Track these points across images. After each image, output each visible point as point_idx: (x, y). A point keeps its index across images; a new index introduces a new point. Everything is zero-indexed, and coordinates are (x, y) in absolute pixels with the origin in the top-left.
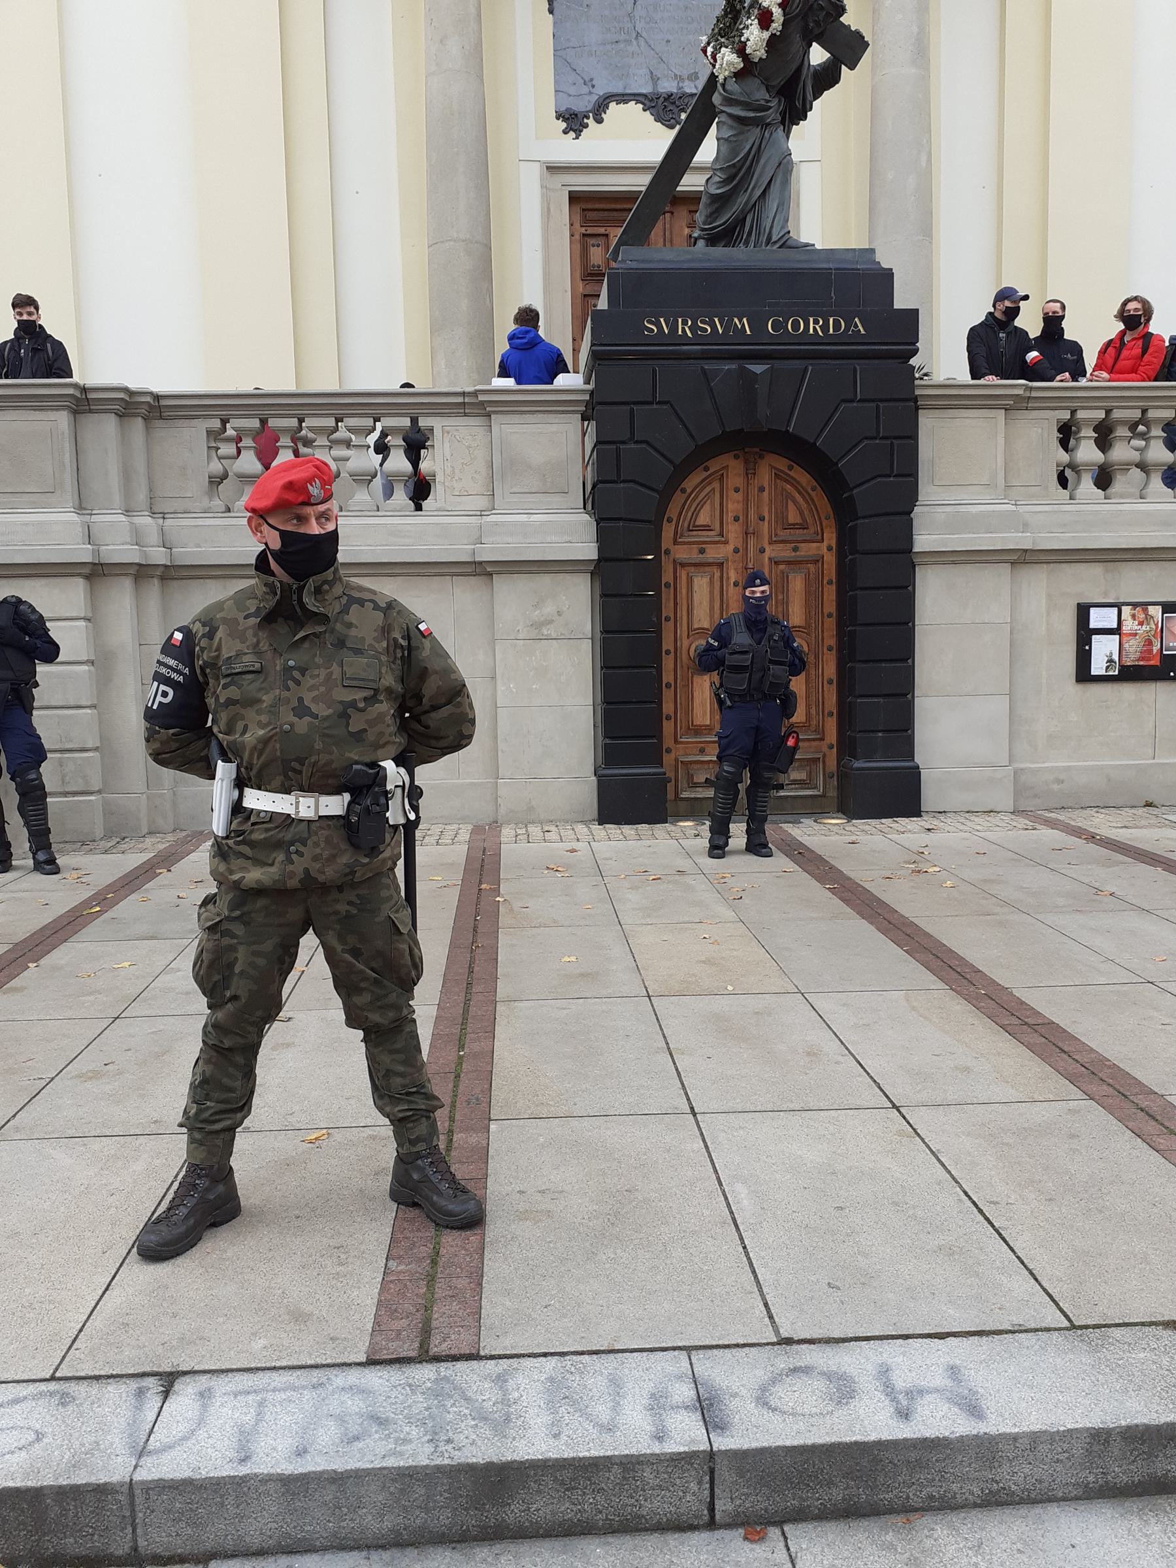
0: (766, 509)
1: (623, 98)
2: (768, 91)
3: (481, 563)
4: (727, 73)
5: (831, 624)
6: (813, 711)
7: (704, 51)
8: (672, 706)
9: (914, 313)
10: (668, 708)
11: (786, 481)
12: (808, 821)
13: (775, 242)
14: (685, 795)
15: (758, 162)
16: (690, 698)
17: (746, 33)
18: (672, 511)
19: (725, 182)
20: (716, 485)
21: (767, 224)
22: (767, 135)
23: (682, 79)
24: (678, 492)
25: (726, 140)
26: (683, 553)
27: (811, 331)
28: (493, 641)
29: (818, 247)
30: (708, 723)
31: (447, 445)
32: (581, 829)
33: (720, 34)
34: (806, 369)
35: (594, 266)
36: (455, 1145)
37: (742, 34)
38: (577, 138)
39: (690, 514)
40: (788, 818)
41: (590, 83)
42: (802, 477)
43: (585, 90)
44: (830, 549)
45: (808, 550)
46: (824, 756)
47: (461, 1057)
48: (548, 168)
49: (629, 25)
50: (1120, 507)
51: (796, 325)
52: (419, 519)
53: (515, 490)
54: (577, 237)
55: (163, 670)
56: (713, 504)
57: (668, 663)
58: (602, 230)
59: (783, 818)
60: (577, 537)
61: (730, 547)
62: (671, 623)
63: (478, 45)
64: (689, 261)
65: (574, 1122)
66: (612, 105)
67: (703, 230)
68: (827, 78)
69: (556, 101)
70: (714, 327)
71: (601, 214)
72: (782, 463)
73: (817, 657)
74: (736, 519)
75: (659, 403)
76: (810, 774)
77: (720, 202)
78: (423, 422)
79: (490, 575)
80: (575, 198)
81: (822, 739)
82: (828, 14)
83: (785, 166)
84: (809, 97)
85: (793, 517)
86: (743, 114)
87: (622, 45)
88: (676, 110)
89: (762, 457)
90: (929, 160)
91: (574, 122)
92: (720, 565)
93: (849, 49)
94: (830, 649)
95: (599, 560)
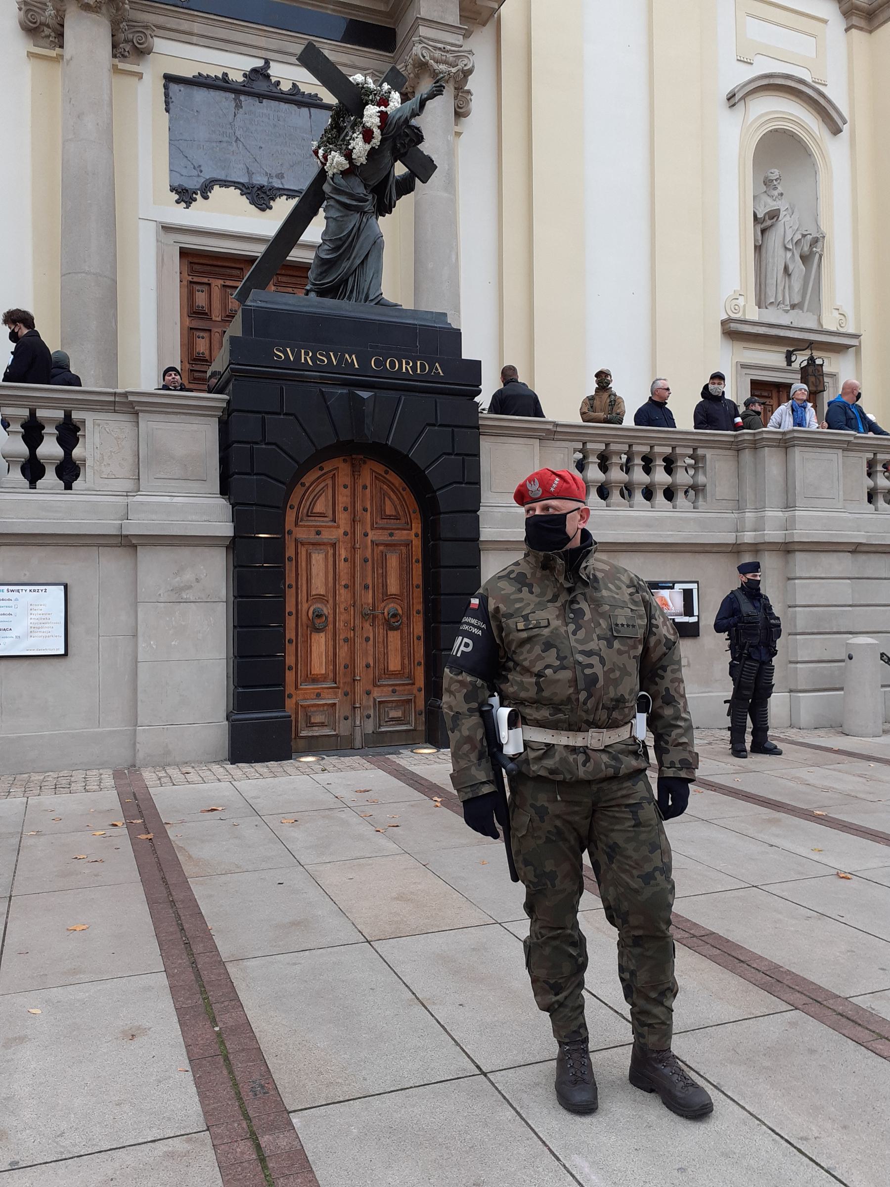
0: (369, 503)
1: (225, 184)
2: (366, 188)
3: (127, 536)
4: (335, 170)
5: (418, 594)
6: (406, 662)
7: (316, 153)
8: (293, 658)
9: (478, 364)
10: (290, 660)
11: (384, 483)
12: (406, 752)
14: (304, 733)
15: (358, 238)
16: (308, 652)
17: (353, 144)
18: (294, 500)
20: (330, 482)
22: (365, 220)
23: (271, 176)
24: (299, 485)
25: (335, 219)
26: (302, 534)
27: (404, 370)
28: (135, 604)
29: (403, 307)
30: (323, 672)
31: (97, 435)
32: (215, 767)
33: (328, 142)
34: (400, 399)
35: (198, 306)
36: (267, 1153)
37: (350, 144)
38: (187, 208)
39: (308, 503)
40: (391, 749)
41: (199, 168)
42: (397, 481)
43: (195, 173)
44: (416, 535)
45: (401, 535)
46: (415, 697)
47: (219, 1034)
48: (163, 227)
49: (231, 131)
50: (618, 513)
51: (392, 364)
52: (33, 496)
53: (158, 476)
54: (185, 283)
55: (749, 739)
56: (327, 496)
57: (290, 622)
58: (205, 280)
59: (386, 749)
60: (214, 516)
61: (341, 531)
62: (293, 590)
63: (110, 124)
64: (308, 306)
65: (376, 1102)
66: (216, 187)
67: (314, 284)
68: (406, 186)
70: (329, 359)
71: (209, 268)
72: (380, 468)
73: (409, 618)
74: (345, 509)
75: (286, 414)
76: (404, 713)
77: (326, 265)
78: (75, 415)
79: (135, 547)
80: (184, 253)
81: (413, 684)
82: (411, 140)
83: (377, 244)
84: (394, 198)
85: (389, 510)
86: (348, 201)
87: (225, 145)
88: (266, 198)
89: (365, 463)
90: (457, 259)
91: (185, 196)
92: (334, 545)
93: (423, 168)
94: (418, 612)
95: (234, 537)
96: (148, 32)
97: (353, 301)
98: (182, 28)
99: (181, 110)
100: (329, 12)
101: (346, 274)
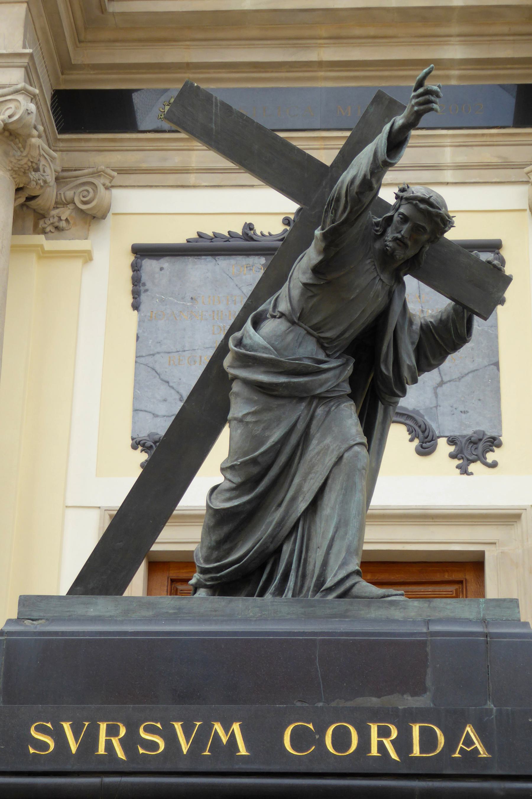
13: (330, 590)
19: (240, 489)
21: (316, 558)
27: (374, 751)
51: (341, 740)
67: (204, 571)
69: (134, 423)
70: (59, 736)
96: (99, 182)
97: (268, 596)
98: (168, 164)
99: (162, 301)
100: (454, 82)
101: (273, 537)
